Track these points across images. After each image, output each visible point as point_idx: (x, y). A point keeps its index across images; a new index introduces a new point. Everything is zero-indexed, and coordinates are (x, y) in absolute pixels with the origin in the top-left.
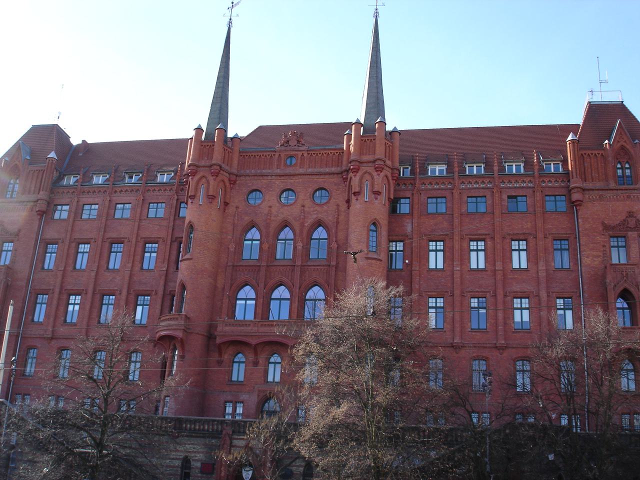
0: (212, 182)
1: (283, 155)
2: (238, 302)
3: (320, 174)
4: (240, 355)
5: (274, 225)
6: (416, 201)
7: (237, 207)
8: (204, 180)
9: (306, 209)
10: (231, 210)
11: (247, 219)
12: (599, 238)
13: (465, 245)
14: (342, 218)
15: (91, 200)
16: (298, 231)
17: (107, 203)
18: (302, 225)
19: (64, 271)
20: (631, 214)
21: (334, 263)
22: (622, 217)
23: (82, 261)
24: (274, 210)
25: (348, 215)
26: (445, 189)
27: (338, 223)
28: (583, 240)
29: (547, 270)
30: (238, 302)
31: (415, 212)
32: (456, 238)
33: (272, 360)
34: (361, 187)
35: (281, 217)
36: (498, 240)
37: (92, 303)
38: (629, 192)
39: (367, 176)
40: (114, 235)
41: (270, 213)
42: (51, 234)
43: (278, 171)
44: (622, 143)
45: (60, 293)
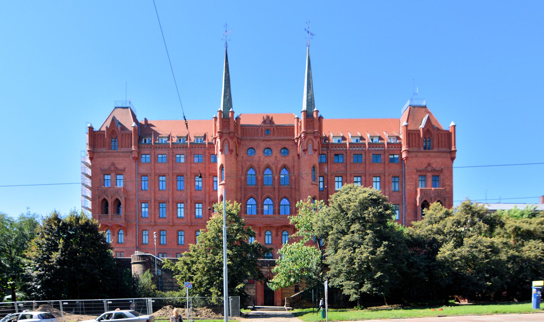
0: (231, 142)
1: (263, 129)
2: (248, 206)
3: (283, 140)
4: (285, 232)
5: (262, 168)
6: (329, 156)
7: (243, 157)
8: (226, 141)
9: (278, 159)
10: (240, 158)
11: (248, 164)
12: (415, 176)
13: (352, 179)
14: (296, 164)
15: (161, 152)
16: (274, 170)
17: (171, 154)
18: (276, 167)
19: (155, 190)
20: (429, 165)
21: (293, 187)
22: (425, 166)
23: (163, 186)
24: (262, 159)
25: (299, 162)
26: (343, 150)
27: (294, 166)
28: (407, 177)
29: (389, 192)
30: (248, 206)
31: (329, 162)
32: (348, 175)
33: (284, 234)
34: (307, 147)
35: (265, 163)
36: (367, 177)
37: (173, 207)
38: (429, 153)
39: (310, 141)
40: (178, 172)
41: (259, 161)
42: (143, 170)
43: (262, 138)
44: (428, 127)
45: (155, 202)
